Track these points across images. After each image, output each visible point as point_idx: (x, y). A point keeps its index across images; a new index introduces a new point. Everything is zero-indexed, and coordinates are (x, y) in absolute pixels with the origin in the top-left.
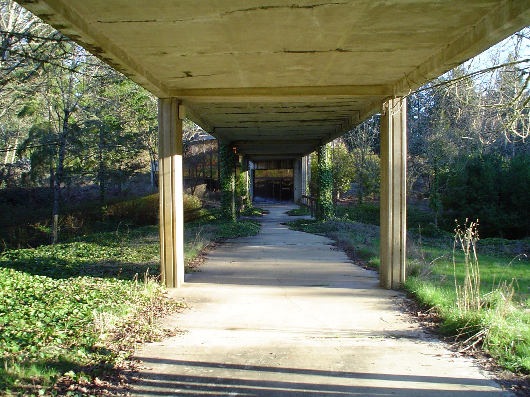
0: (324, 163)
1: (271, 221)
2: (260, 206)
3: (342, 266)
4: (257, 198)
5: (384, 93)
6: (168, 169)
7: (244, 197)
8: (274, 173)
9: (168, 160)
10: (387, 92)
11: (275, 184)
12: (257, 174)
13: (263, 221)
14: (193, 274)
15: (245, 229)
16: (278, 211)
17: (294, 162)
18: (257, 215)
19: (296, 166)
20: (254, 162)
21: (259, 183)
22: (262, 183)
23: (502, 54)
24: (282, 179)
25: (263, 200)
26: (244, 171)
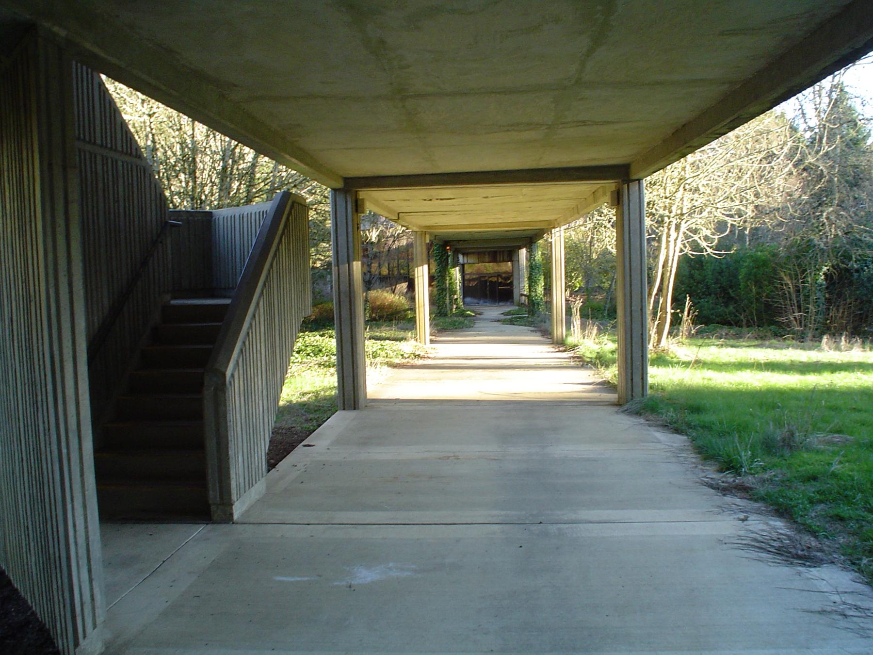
0: (534, 260)
1: (485, 320)
2: (473, 308)
3: (537, 337)
4: (468, 299)
5: (549, 225)
6: (420, 274)
7: (456, 297)
8: (490, 268)
9: (420, 268)
10: (550, 226)
11: (491, 282)
12: (468, 270)
13: (477, 320)
14: (432, 341)
15: (461, 323)
16: (494, 311)
17: (510, 254)
18: (470, 316)
19: (515, 259)
20: (463, 254)
21: (470, 280)
22: (473, 280)
23: (581, 223)
24: (499, 275)
25: (476, 301)
26: (454, 267)
